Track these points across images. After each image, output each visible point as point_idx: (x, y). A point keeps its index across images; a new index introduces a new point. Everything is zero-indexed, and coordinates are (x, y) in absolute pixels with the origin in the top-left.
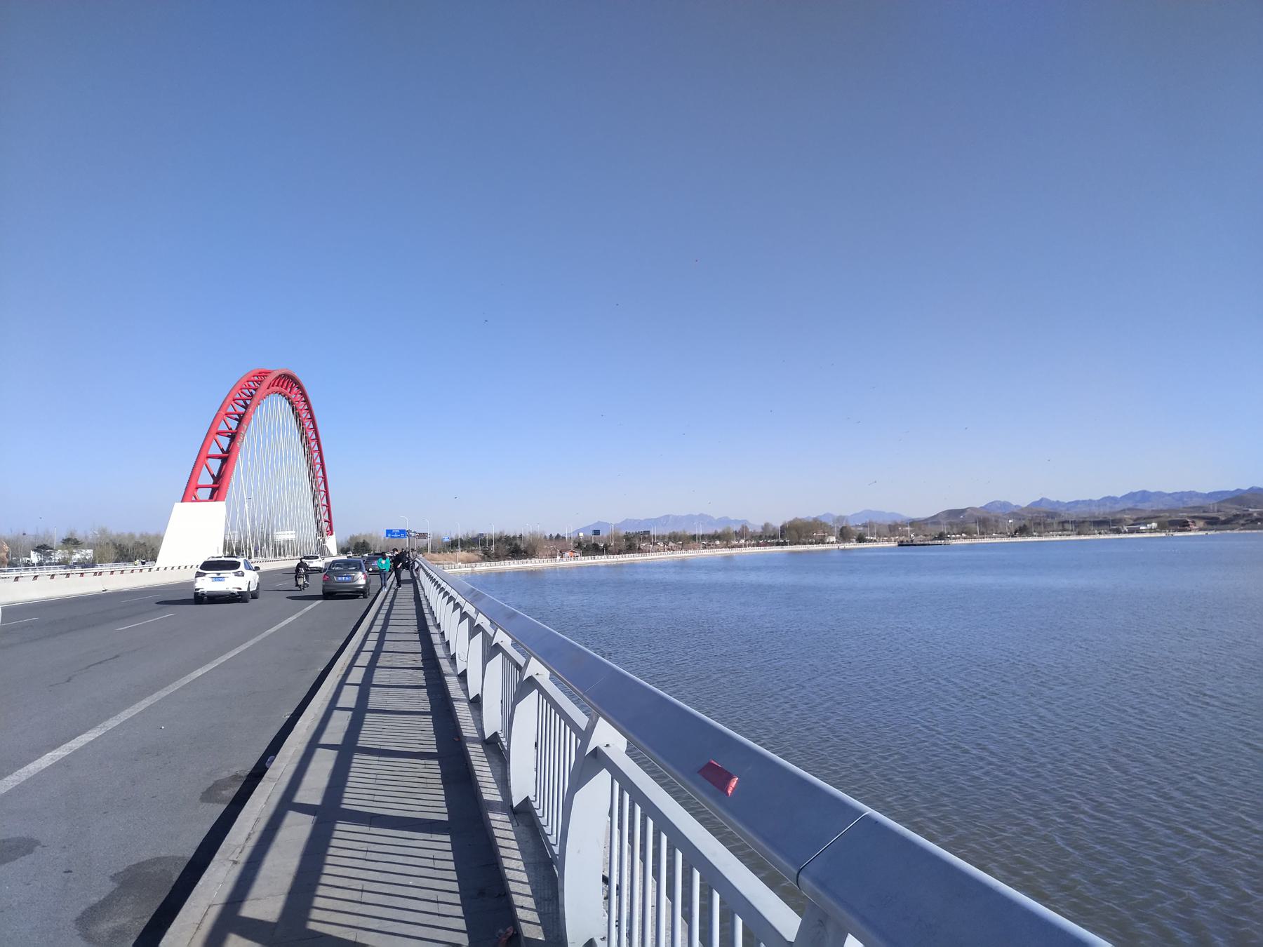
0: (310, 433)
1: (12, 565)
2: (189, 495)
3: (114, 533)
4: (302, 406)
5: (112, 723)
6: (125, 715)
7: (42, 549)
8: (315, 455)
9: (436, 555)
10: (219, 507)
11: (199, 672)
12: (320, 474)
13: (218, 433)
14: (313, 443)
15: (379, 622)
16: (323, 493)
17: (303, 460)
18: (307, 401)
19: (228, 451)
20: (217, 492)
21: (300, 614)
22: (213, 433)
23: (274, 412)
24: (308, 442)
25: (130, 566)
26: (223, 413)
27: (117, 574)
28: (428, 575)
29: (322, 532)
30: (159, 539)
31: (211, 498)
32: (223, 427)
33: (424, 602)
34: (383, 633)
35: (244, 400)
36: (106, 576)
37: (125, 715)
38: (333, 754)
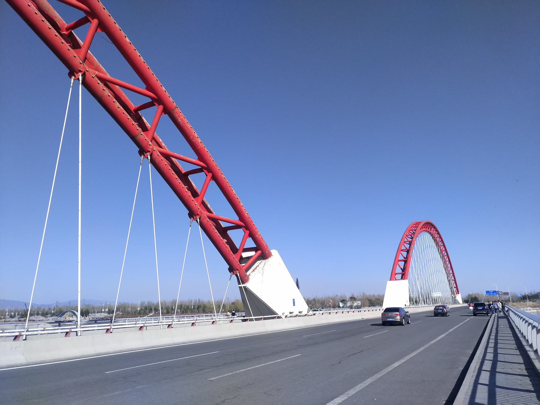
0: (442, 247)
1: (334, 307)
2: (393, 277)
3: (368, 295)
4: (436, 236)
5: (352, 392)
6: (358, 388)
7: (343, 301)
8: (446, 257)
9: (515, 304)
10: (405, 282)
11: (396, 364)
12: (449, 265)
13: (402, 250)
14: (444, 252)
15: (492, 341)
16: (451, 275)
17: (440, 260)
18: (438, 233)
19: (407, 258)
20: (404, 276)
21: (447, 333)
22: (399, 250)
23: (424, 240)
24: (442, 252)
25: (374, 308)
26: (403, 242)
27: (367, 312)
28: (516, 314)
29: (453, 293)
30: (384, 296)
31: (402, 278)
32: (403, 248)
33: (516, 330)
34: (496, 348)
35: (411, 235)
36: (362, 312)
37: (358, 388)
38: (488, 373)
